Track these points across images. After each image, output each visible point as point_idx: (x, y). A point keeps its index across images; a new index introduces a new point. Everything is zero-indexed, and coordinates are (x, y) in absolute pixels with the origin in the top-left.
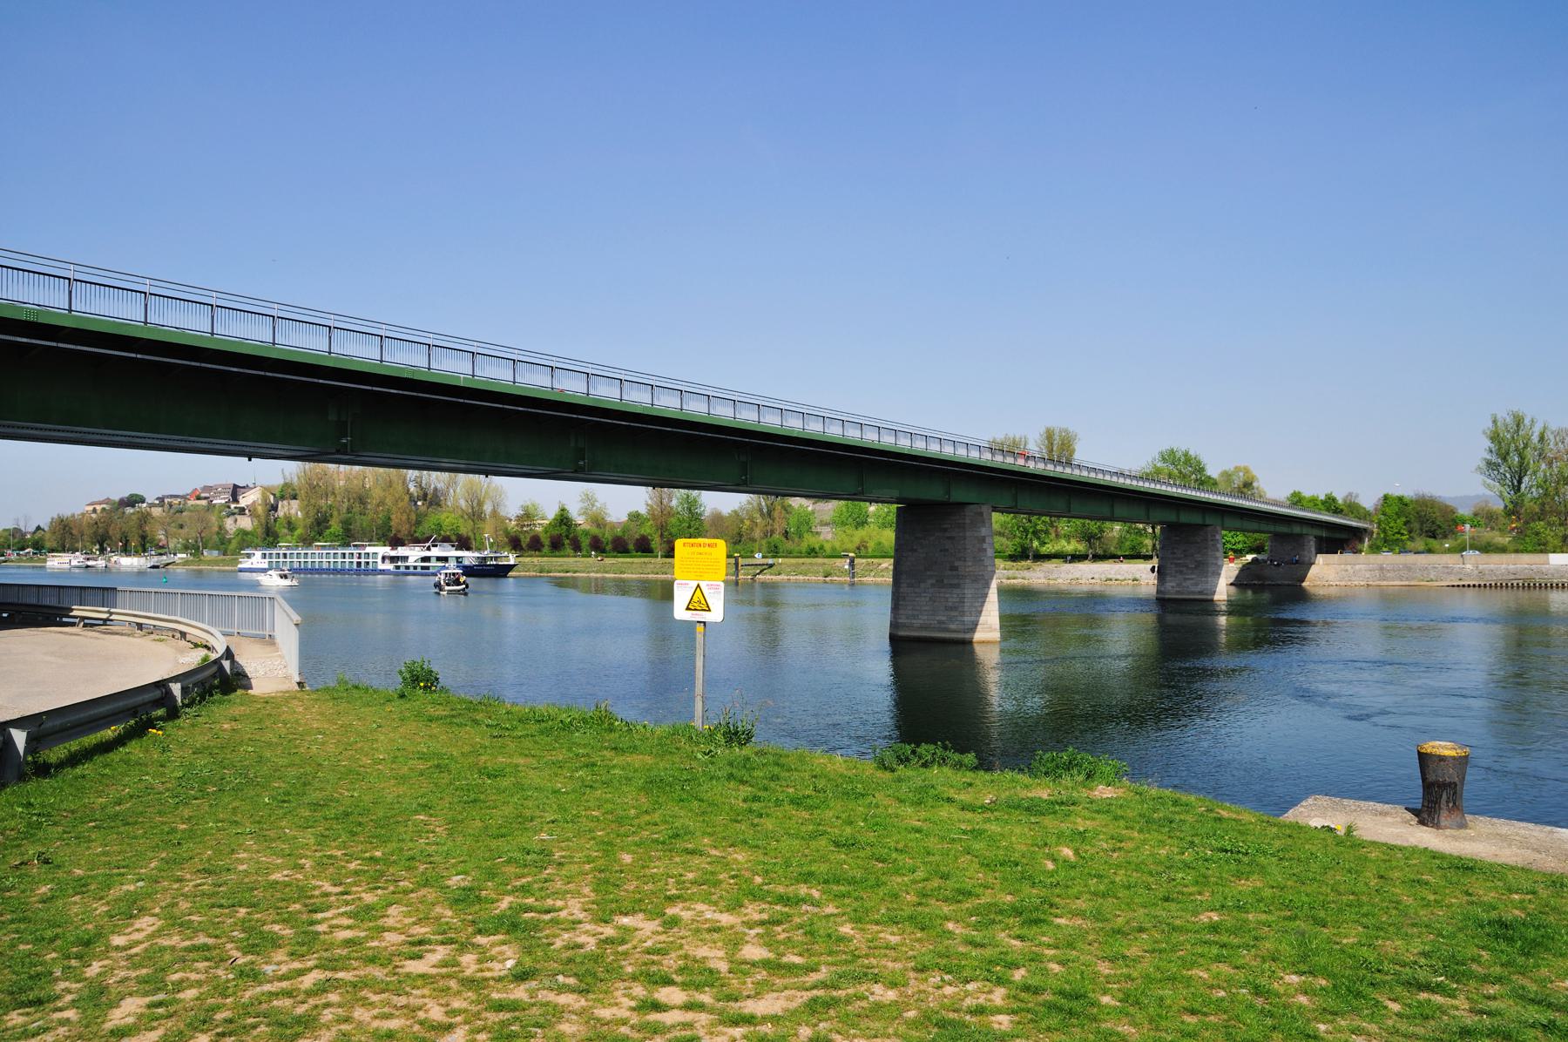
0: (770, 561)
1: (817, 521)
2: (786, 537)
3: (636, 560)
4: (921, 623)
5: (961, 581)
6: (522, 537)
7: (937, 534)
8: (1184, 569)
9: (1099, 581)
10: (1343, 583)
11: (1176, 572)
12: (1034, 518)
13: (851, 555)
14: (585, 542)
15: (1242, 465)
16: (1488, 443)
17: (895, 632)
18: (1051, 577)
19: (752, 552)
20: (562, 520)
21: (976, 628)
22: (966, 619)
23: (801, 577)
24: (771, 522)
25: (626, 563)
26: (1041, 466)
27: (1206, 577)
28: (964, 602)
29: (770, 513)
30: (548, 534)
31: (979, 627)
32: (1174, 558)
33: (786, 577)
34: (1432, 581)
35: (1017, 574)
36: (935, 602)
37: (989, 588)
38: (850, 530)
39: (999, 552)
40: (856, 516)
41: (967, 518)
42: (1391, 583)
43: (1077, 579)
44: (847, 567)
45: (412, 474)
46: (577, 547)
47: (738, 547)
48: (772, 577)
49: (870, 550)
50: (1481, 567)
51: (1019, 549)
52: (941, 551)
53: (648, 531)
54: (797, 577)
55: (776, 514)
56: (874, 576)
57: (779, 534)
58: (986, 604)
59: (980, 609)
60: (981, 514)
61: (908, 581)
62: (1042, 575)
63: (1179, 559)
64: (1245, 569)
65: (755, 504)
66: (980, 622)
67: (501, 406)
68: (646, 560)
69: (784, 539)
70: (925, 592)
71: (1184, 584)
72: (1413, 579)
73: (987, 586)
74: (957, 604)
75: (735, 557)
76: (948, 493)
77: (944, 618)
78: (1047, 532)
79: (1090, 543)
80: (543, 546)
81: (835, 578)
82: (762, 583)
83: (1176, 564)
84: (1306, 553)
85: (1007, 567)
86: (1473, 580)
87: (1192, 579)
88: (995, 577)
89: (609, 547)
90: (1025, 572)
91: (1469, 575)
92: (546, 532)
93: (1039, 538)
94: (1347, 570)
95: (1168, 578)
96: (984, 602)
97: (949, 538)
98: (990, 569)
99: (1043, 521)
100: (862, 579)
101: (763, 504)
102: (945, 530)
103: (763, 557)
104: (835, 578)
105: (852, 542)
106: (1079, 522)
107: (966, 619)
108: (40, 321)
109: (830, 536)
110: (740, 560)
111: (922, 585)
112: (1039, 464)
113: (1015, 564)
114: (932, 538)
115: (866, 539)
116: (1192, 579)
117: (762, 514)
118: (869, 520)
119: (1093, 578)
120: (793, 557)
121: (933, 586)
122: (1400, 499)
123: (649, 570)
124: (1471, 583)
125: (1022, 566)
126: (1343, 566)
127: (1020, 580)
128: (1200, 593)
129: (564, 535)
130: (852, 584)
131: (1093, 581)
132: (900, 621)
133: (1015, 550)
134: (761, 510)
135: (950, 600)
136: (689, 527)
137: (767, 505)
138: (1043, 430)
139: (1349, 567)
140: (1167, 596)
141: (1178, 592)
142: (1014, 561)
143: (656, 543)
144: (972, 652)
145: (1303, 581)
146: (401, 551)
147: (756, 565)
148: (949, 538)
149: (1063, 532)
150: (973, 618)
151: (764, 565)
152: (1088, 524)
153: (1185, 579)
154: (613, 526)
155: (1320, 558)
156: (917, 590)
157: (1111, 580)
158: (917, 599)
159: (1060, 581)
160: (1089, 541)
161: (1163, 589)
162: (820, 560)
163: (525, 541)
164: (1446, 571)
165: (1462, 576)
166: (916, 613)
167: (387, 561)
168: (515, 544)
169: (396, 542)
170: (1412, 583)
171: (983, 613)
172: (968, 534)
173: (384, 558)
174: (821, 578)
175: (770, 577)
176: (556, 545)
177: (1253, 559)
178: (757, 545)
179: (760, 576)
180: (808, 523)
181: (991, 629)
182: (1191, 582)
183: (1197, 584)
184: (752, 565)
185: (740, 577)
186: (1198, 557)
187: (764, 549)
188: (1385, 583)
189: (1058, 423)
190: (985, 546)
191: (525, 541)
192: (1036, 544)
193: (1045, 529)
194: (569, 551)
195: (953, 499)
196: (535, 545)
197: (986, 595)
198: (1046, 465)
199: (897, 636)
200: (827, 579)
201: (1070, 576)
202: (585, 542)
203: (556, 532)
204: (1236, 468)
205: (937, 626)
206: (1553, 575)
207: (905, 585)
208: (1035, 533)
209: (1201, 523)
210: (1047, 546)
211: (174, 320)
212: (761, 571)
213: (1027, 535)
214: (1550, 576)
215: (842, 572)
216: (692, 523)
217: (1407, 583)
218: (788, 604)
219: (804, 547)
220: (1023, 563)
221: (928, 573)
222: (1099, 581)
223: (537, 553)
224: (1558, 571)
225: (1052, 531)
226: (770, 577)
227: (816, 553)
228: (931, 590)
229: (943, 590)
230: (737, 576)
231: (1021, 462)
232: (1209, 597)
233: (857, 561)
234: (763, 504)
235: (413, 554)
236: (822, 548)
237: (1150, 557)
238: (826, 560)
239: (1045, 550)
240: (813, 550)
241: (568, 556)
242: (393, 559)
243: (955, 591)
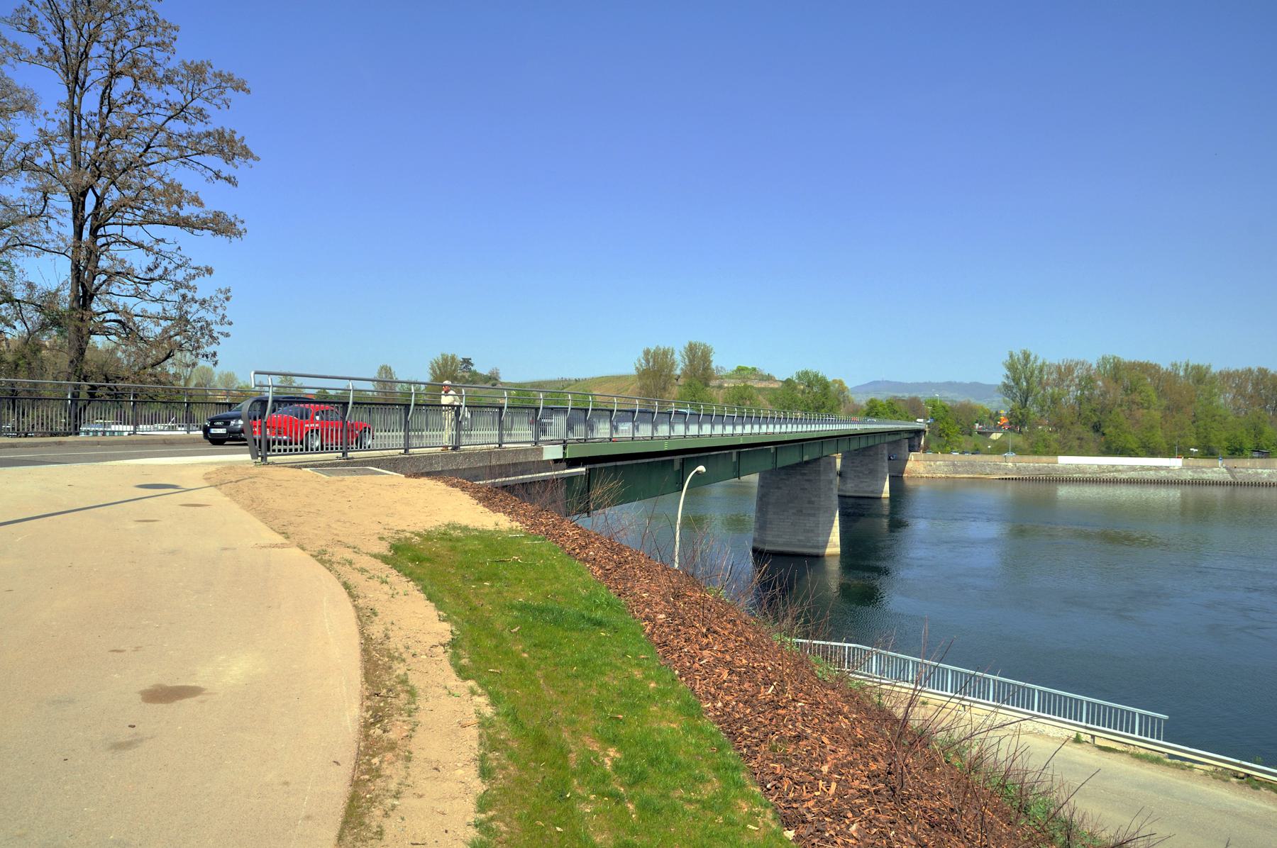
4: (782, 539)
8: (860, 474)
10: (930, 475)
11: (855, 476)
15: (837, 378)
16: (1006, 372)
27: (877, 480)
32: (853, 467)
34: (988, 474)
42: (962, 476)
50: (1018, 465)
63: (857, 467)
70: (788, 519)
72: (976, 473)
77: (803, 538)
83: (855, 471)
86: (1014, 474)
87: (866, 482)
91: (1011, 470)
94: (931, 466)
95: (849, 481)
96: (832, 526)
107: (820, 539)
116: (866, 482)
124: (1014, 477)
126: (928, 462)
128: (872, 492)
135: (808, 525)
139: (932, 463)
153: (862, 482)
161: (844, 488)
170: (975, 476)
172: (822, 478)
181: (835, 546)
182: (866, 484)
183: (870, 486)
189: (700, 338)
204: (834, 381)
206: (1062, 471)
217: (972, 476)
221: (790, 505)
224: (1064, 468)
229: (802, 518)
232: (879, 496)
243: (811, 518)
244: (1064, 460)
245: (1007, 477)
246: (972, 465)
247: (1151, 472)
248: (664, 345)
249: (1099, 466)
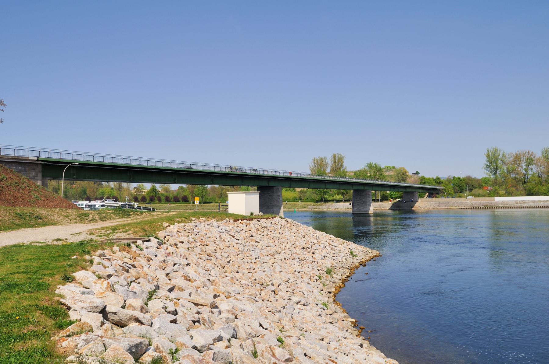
3: (182, 205)
6: (138, 196)
14: (163, 198)
16: (486, 158)
20: (153, 190)
25: (179, 206)
27: (366, 206)
30: (148, 196)
35: (317, 207)
45: (134, 185)
46: (160, 200)
47: (221, 199)
50: (472, 202)
51: (320, 198)
53: (187, 194)
60: (278, 189)
62: (326, 207)
63: (358, 200)
64: (394, 204)
68: (186, 204)
71: (360, 209)
75: (219, 203)
80: (147, 200)
84: (415, 198)
86: (469, 206)
89: (172, 200)
91: (467, 205)
92: (147, 195)
110: (221, 204)
113: (317, 203)
121: (266, 208)
122: (459, 178)
123: (188, 208)
128: (365, 211)
129: (154, 195)
136: (202, 192)
138: (332, 155)
139: (429, 203)
140: (355, 213)
141: (358, 211)
142: (317, 202)
143: (190, 198)
145: (413, 208)
146: (92, 203)
153: (360, 207)
154: (173, 192)
155: (420, 200)
157: (349, 208)
163: (140, 198)
164: (461, 203)
165: (465, 205)
167: (87, 207)
168: (136, 199)
169: (89, 199)
172: (275, 194)
173: (86, 206)
176: (152, 200)
177: (398, 201)
183: (364, 208)
185: (221, 210)
186: (364, 200)
188: (440, 208)
189: (338, 152)
190: (280, 197)
191: (140, 198)
194: (157, 202)
196: (144, 199)
201: (336, 207)
202: (163, 198)
203: (151, 195)
209: (363, 189)
214: (493, 204)
216: (203, 191)
217: (447, 208)
220: (320, 203)
223: (144, 203)
230: (220, 209)
235: (98, 204)
237: (349, 201)
241: (157, 204)
242: (90, 206)
244: (497, 199)
245: (466, 207)
246: (449, 203)
247: (542, 203)
248: (323, 156)
249: (515, 201)
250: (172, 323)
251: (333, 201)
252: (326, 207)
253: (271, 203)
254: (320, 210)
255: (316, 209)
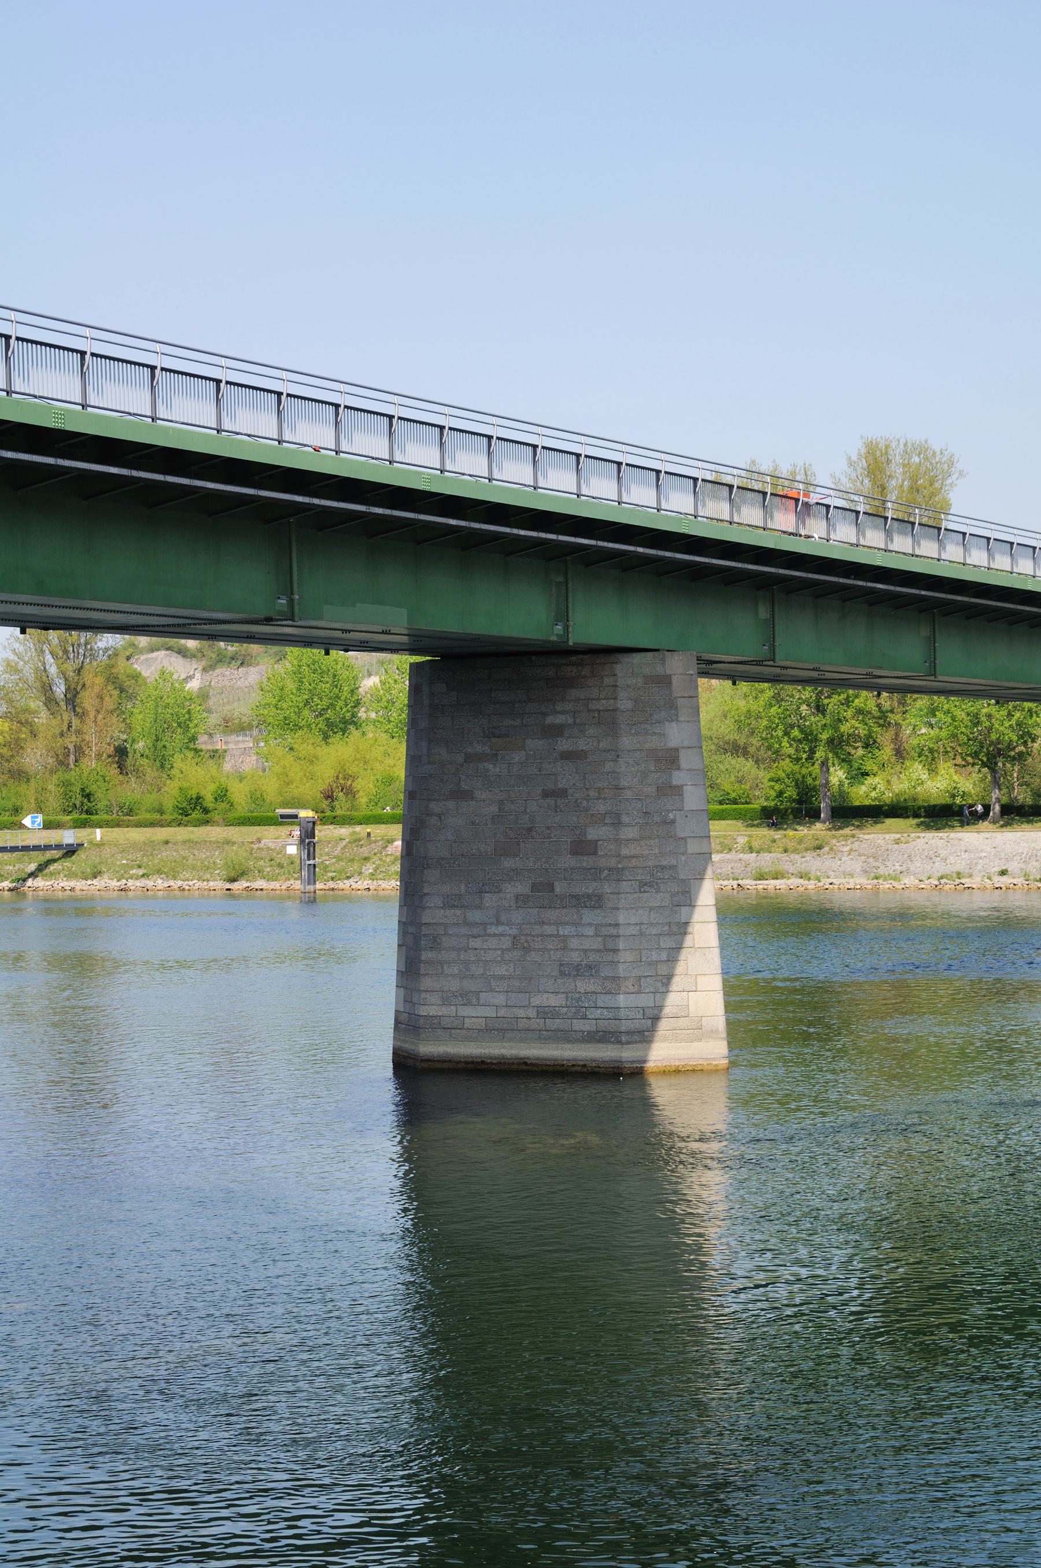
0: (68, 837)
1: (213, 719)
2: (121, 767)
5: (607, 888)
7: (530, 743)
9: (1020, 881)
12: (832, 703)
13: (305, 814)
17: (407, 1046)
18: (882, 871)
19: (17, 811)
21: (653, 1029)
22: (622, 1000)
23: (161, 883)
24: (76, 722)
26: (845, 532)
28: (616, 951)
29: (72, 698)
31: (663, 1025)
33: (114, 884)
36: (527, 950)
37: (692, 905)
38: (307, 743)
39: (735, 802)
40: (326, 702)
41: (622, 694)
43: (959, 875)
44: (292, 850)
48: (72, 883)
49: (363, 800)
51: (791, 792)
52: (546, 794)
54: (149, 883)
55: (87, 701)
56: (372, 877)
57: (99, 756)
58: (684, 954)
59: (663, 969)
60: (665, 681)
61: (446, 889)
62: (857, 866)
65: (28, 672)
66: (667, 1010)
67: (362, 508)
69: (114, 770)
70: (499, 923)
73: (686, 899)
74: (593, 957)
76: (563, 616)
77: (554, 1001)
78: (870, 744)
79: (993, 771)
81: (260, 883)
82: (46, 900)
85: (756, 845)
88: (709, 873)
90: (809, 856)
93: (846, 761)
96: (679, 948)
97: (568, 756)
98: (692, 847)
99: (860, 711)
100: (340, 885)
101: (53, 670)
102: (556, 731)
103: (48, 826)
104: (260, 883)
105: (312, 777)
106: (960, 708)
107: (622, 1000)
108: (66, 429)
109: (249, 764)
111: (489, 900)
112: (923, 543)
113: (777, 835)
114: (518, 757)
115: (352, 770)
117: (50, 701)
118: (362, 714)
119: (1003, 873)
120: (139, 825)
121: (522, 901)
125: (800, 841)
127: (794, 882)
130: (311, 900)
131: (1005, 880)
132: (423, 1011)
133: (780, 794)
134: (47, 688)
135: (574, 943)
137: (63, 673)
142: (774, 825)
144: (647, 1105)
147: (26, 849)
148: (568, 756)
149: (915, 742)
150: (646, 1000)
151: (48, 847)
152: (989, 716)
156: (475, 916)
158: (473, 943)
159: (908, 881)
160: (990, 764)
162: (215, 833)
166: (470, 985)
171: (677, 983)
172: (627, 742)
174: (220, 885)
175: (68, 884)
178: (29, 792)
179: (39, 882)
180: (184, 726)
184: (14, 849)
187: (54, 802)
190: (678, 778)
192: (838, 775)
193: (863, 732)
195: (574, 639)
197: (682, 929)
198: (916, 542)
199: (415, 1057)
200: (235, 886)
201: (939, 868)
205: (537, 1023)
207: (438, 901)
208: (836, 744)
210: (870, 780)
211: (114, 402)
212: (41, 868)
213: (812, 752)
215: (280, 866)
218: (117, 964)
219: (171, 794)
220: (803, 831)
221: (508, 863)
222: (1020, 881)
225: (885, 738)
226: (68, 884)
227: (206, 811)
228: (517, 916)
229: (552, 914)
231: (784, 520)
233: (322, 832)
234: (53, 670)
236: (222, 795)
238: (235, 833)
239: (862, 794)
240: (197, 802)
243: (589, 916)
250: (47, 829)
251: (896, 810)
252: (857, 866)
253: (583, 847)
254: (811, 885)
255: (780, 883)
